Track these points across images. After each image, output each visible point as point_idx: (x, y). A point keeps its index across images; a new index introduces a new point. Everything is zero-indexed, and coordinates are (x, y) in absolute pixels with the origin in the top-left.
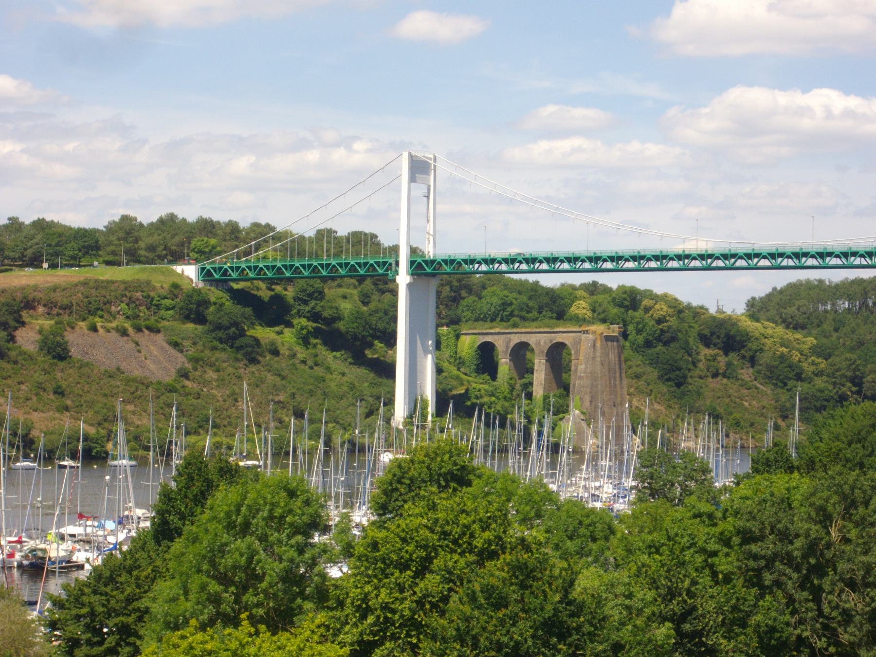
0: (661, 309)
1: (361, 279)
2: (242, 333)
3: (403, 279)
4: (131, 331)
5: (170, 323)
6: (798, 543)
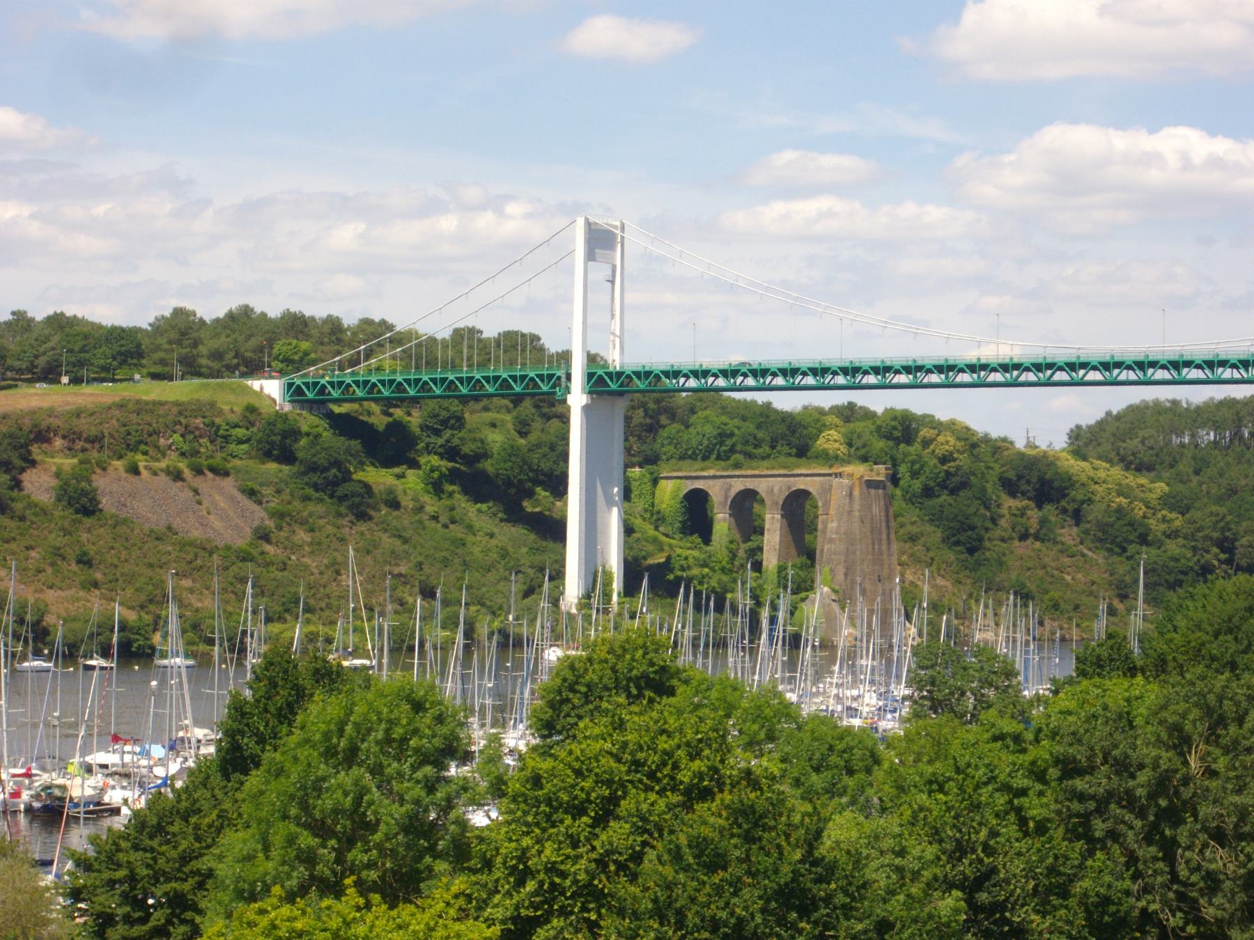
0: (947, 442)
1: (517, 399)
2: (347, 477)
3: (577, 399)
4: (187, 473)
5: (244, 462)
6: (1143, 777)
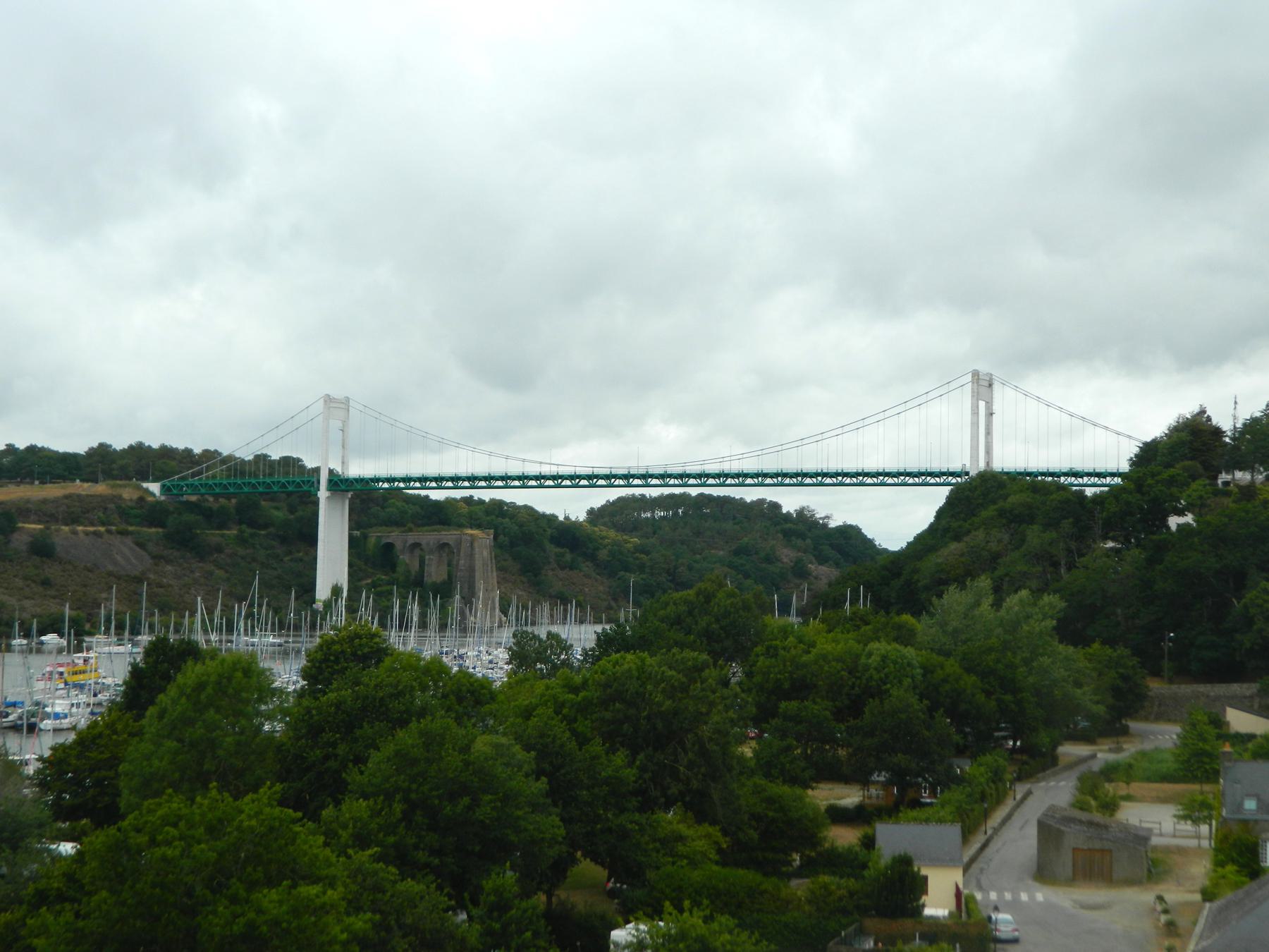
3: (323, 494)
